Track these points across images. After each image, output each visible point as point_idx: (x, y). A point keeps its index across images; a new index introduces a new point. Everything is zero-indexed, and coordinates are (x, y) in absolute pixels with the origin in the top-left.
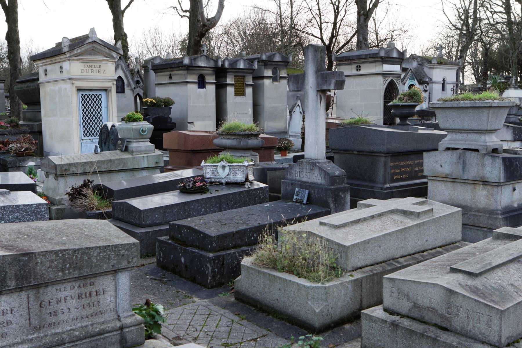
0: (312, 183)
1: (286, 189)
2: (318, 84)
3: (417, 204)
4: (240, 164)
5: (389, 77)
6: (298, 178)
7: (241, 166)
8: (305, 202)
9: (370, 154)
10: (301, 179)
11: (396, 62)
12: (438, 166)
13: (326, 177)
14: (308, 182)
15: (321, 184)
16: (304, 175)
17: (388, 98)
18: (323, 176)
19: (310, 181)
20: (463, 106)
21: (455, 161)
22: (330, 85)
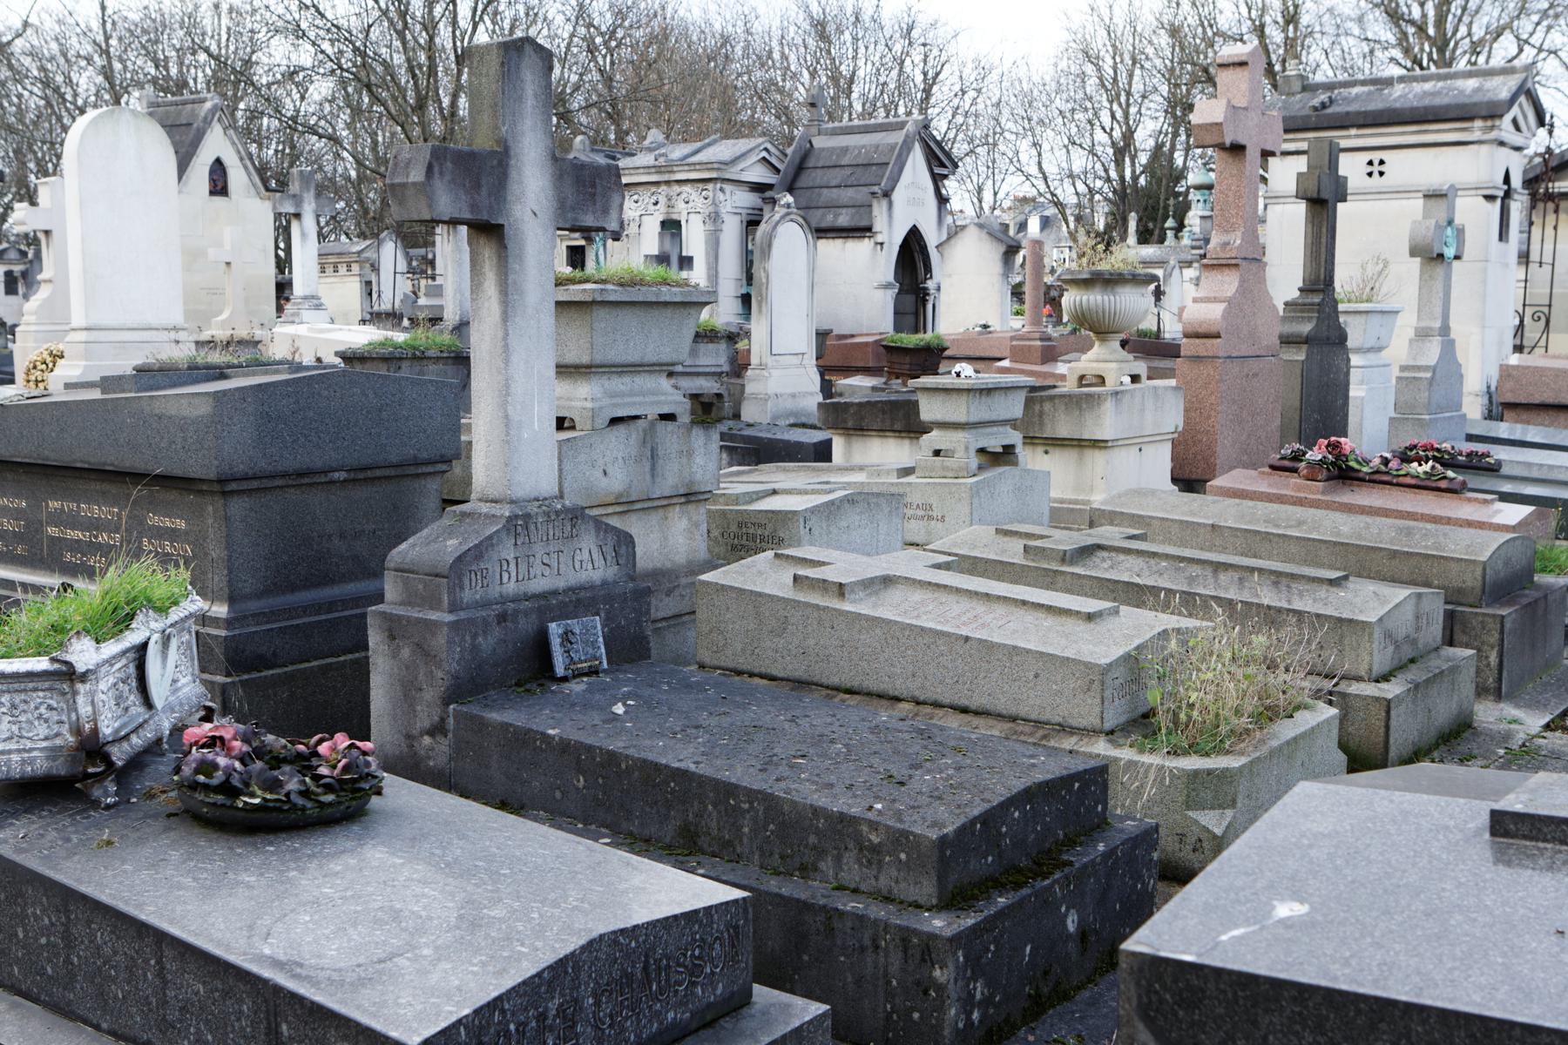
0: (571, 589)
1: (475, 648)
2: (562, 207)
3: (1042, 537)
6: (511, 587)
9: (399, 471)
12: (598, 474)
14: (555, 593)
15: (604, 583)
16: (538, 569)
18: (609, 550)
19: (561, 584)
20: (668, 299)
21: (633, 453)
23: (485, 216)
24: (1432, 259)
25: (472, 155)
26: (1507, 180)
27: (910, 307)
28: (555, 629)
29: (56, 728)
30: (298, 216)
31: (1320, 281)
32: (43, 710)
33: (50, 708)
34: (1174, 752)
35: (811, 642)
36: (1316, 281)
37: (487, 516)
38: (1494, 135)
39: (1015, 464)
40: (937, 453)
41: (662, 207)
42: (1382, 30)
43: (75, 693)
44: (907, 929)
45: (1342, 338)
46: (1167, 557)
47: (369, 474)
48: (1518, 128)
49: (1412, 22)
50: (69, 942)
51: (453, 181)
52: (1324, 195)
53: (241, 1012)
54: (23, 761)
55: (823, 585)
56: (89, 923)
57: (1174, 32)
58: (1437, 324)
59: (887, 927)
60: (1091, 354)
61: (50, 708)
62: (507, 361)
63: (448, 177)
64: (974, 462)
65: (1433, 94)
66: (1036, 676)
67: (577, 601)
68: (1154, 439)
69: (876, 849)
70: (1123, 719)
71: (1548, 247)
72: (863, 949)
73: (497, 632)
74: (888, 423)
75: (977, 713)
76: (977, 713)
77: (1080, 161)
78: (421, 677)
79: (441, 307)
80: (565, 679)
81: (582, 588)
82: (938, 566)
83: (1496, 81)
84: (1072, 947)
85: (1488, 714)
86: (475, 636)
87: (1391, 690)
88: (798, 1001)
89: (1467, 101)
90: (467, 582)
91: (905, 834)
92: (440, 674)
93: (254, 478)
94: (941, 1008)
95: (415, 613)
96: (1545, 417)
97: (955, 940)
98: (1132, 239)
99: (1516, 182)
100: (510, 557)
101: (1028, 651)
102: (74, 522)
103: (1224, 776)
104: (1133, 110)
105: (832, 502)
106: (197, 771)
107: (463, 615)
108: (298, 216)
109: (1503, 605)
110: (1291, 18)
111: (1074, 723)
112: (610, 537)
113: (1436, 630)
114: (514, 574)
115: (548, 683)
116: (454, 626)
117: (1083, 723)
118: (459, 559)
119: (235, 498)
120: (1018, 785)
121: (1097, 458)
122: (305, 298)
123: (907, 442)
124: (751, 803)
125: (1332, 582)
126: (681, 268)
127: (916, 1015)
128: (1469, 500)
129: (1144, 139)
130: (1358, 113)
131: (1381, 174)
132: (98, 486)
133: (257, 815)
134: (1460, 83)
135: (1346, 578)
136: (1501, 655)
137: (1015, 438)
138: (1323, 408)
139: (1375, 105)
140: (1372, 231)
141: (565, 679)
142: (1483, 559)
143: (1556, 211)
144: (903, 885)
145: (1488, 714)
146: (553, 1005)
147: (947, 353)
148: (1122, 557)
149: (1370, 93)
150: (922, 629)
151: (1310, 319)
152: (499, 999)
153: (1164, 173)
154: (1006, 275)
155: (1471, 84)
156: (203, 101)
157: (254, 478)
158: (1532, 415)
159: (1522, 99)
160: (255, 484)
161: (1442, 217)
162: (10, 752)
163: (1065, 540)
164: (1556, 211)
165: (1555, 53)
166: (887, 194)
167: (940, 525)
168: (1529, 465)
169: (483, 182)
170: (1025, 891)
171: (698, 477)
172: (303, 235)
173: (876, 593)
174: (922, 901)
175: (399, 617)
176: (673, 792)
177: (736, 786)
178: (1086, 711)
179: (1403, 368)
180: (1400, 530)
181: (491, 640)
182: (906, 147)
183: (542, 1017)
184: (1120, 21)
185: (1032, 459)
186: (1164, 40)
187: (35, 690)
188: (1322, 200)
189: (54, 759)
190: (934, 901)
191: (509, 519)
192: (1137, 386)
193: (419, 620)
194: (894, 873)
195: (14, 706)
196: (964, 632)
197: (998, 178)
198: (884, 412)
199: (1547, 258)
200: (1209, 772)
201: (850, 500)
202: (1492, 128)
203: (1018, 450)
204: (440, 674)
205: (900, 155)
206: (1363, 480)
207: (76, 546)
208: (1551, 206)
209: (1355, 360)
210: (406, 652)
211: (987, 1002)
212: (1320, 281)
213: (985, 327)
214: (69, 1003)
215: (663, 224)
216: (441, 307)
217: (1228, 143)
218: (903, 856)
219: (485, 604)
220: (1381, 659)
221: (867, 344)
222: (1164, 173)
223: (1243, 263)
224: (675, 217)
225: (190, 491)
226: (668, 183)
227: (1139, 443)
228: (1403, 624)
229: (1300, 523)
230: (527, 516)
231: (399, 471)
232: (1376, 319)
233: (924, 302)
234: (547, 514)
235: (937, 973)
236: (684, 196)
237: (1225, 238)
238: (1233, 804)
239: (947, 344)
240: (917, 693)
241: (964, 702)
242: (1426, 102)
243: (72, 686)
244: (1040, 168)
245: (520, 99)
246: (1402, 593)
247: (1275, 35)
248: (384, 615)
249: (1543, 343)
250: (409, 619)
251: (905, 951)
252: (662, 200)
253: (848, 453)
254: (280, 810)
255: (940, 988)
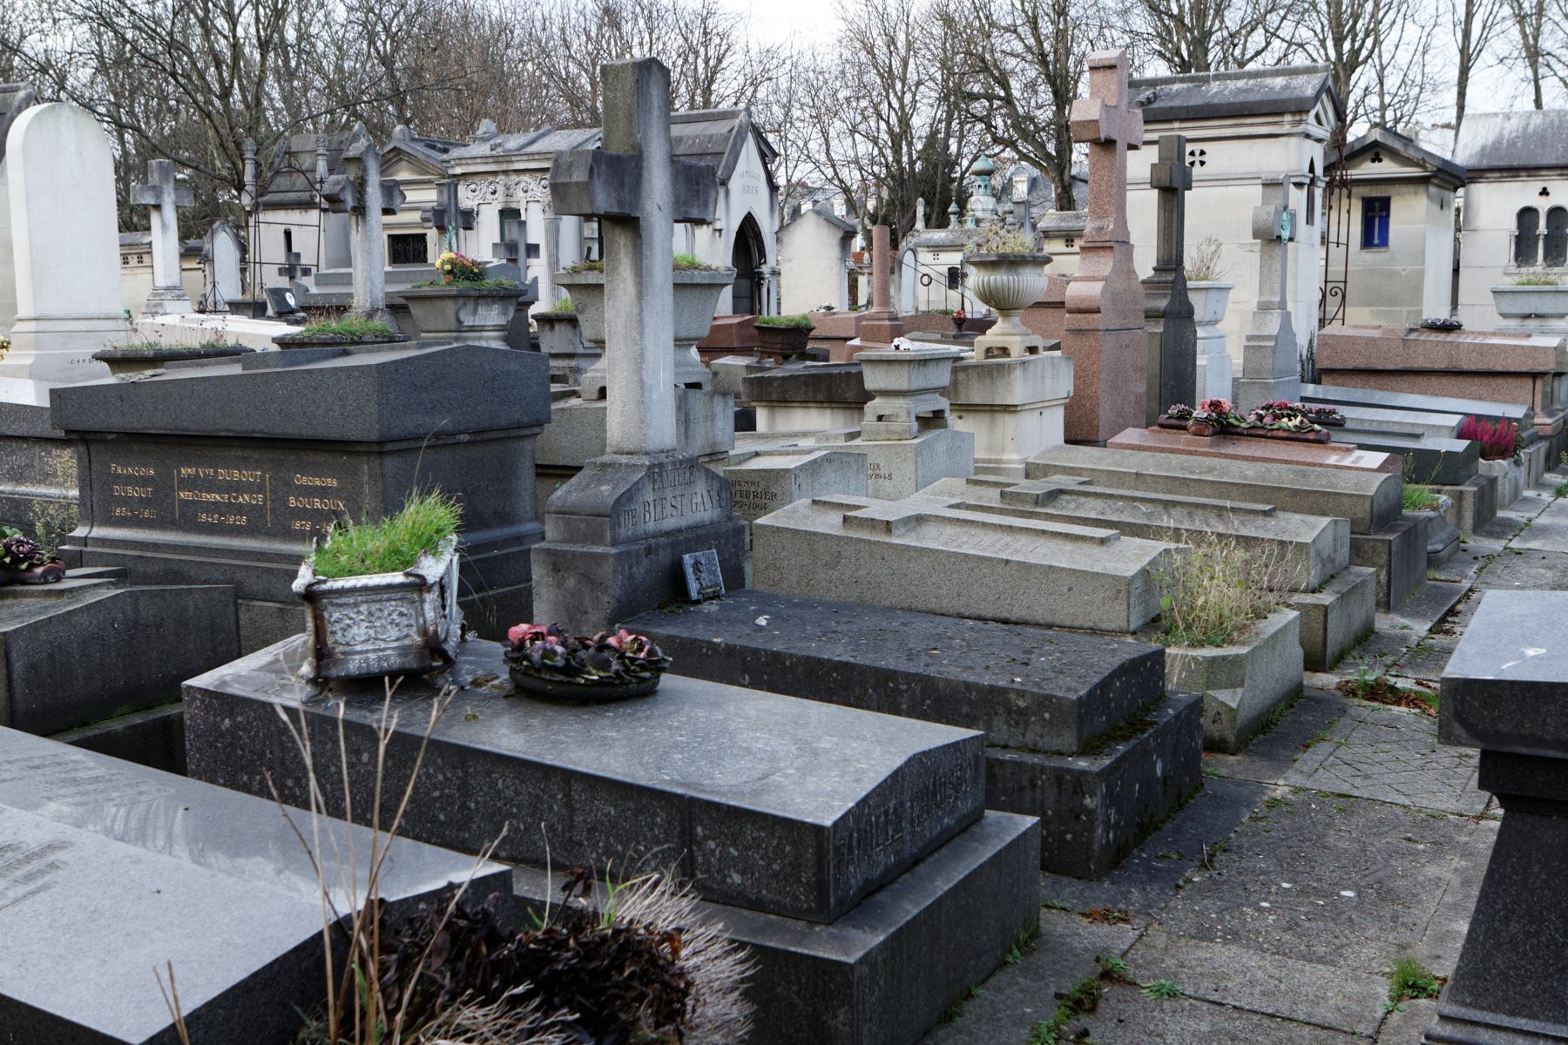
0: (690, 528)
1: (631, 577)
3: (859, 507)
6: (651, 526)
9: (505, 434)
14: (679, 530)
15: (712, 523)
16: (669, 510)
18: (714, 493)
19: (683, 523)
23: (627, 210)
24: (1271, 241)
25: (619, 158)
26: (1312, 169)
27: (745, 292)
29: (405, 631)
30: (158, 207)
31: (1171, 261)
32: (395, 616)
33: (401, 614)
34: (1192, 645)
35: (863, 572)
36: (1169, 261)
37: (627, 466)
38: (1301, 128)
39: (945, 426)
40: (880, 418)
41: (500, 195)
42: (1141, 21)
43: (423, 601)
44: (1061, 769)
45: (1190, 312)
46: (1122, 497)
47: (485, 436)
48: (1319, 122)
49: (1171, 16)
50: (465, 791)
52: (1175, 185)
53: (654, 824)
54: (379, 659)
55: (871, 523)
56: (489, 774)
57: (948, 21)
58: (1277, 299)
59: (1043, 769)
60: (994, 329)
61: (401, 614)
62: (642, 334)
64: (915, 426)
65: (1247, 91)
66: (1070, 589)
67: (696, 537)
68: (1050, 404)
69: (1023, 712)
70: (1141, 622)
71: (1344, 228)
72: (1021, 789)
73: (645, 562)
74: (811, 394)
75: (1016, 623)
76: (1016, 623)
77: (864, 148)
78: (587, 602)
79: (351, 295)
80: (698, 602)
82: (951, 506)
83: (1299, 81)
84: (1159, 788)
85: (1385, 623)
86: (631, 567)
87: (1326, 598)
88: (1018, 817)
89: (1277, 97)
91: (1049, 697)
92: (606, 599)
93: (406, 439)
94: (1091, 828)
95: (579, 548)
96: (1358, 380)
97: (1100, 774)
98: (920, 225)
99: (1319, 171)
101: (1062, 569)
102: (211, 485)
103: (1236, 661)
104: (908, 97)
105: (815, 461)
106: (543, 657)
107: (622, 548)
108: (158, 207)
109: (1387, 532)
110: (1062, 12)
111: (1103, 626)
113: (1345, 551)
115: (686, 607)
116: (618, 556)
117: (1111, 626)
118: (618, 501)
120: (1116, 662)
121: (1007, 421)
122: (168, 289)
123: (828, 412)
124: (909, 684)
125: (1265, 513)
126: (528, 256)
127: (1069, 837)
128: (1334, 449)
129: (921, 123)
130: (1181, 108)
131: (1202, 163)
132: (239, 453)
133: (597, 689)
134: (1269, 81)
135: (1274, 510)
136: (1389, 574)
137: (943, 403)
138: (1176, 375)
139: (1194, 101)
140: (1221, 211)
141: (698, 602)
142: (1371, 493)
143: (1349, 197)
144: (1047, 738)
145: (1385, 623)
146: (892, 804)
147: (813, 334)
148: (1082, 500)
149: (1189, 89)
150: (966, 555)
151: (1165, 295)
152: (867, 797)
153: (938, 158)
154: (843, 260)
155: (1279, 82)
156: (16, 90)
157: (406, 439)
158: (1347, 379)
159: (1324, 96)
161: (1279, 202)
162: (367, 651)
163: (1038, 487)
164: (1349, 197)
165: (1301, 46)
166: (724, 183)
167: (887, 482)
168: (1362, 421)
170: (1133, 741)
171: (719, 439)
172: (164, 226)
173: (914, 529)
174: (1063, 750)
175: (564, 553)
176: (835, 680)
177: (895, 672)
178: (1115, 615)
179: (1249, 338)
180: (1296, 473)
181: (642, 570)
182: (740, 138)
183: (886, 813)
184: (893, 12)
185: (956, 423)
186: (938, 30)
187: (389, 600)
188: (1172, 189)
189: (406, 655)
190: (1075, 749)
191: (650, 467)
192: (1033, 357)
193: (584, 554)
194: (1039, 729)
195: (371, 614)
196: (1004, 556)
197: (791, 165)
198: (806, 385)
199: (1343, 239)
200: (1224, 658)
201: (827, 459)
202: (1300, 122)
203: (947, 414)
204: (606, 599)
205: (734, 145)
206: (1241, 434)
207: (213, 507)
208: (1345, 191)
209: (1200, 333)
210: (571, 582)
211: (1116, 826)
212: (1171, 261)
213: (829, 308)
214: (465, 840)
215: (502, 212)
216: (351, 295)
217: (1103, 137)
218: (1047, 716)
219: (635, 539)
220: (1313, 577)
221: (731, 326)
222: (938, 158)
223: (1117, 246)
224: (514, 206)
225: (343, 453)
226: (506, 172)
227: (1039, 407)
228: (1326, 546)
229: (1211, 470)
230: (661, 465)
231: (505, 434)
232: (1213, 295)
233: (759, 286)
234: (674, 463)
235: (1088, 801)
236: (522, 185)
237: (1099, 224)
238: (1241, 684)
239: (814, 324)
240: (962, 610)
241: (1006, 615)
242: (1241, 98)
243: (421, 595)
244: (828, 153)
245: (649, 111)
246: (1324, 521)
247: (1046, 28)
248: (548, 552)
249: (1340, 315)
250: (574, 554)
251: (1059, 787)
252: (501, 189)
253: (772, 421)
254: (613, 684)
255: (1090, 813)
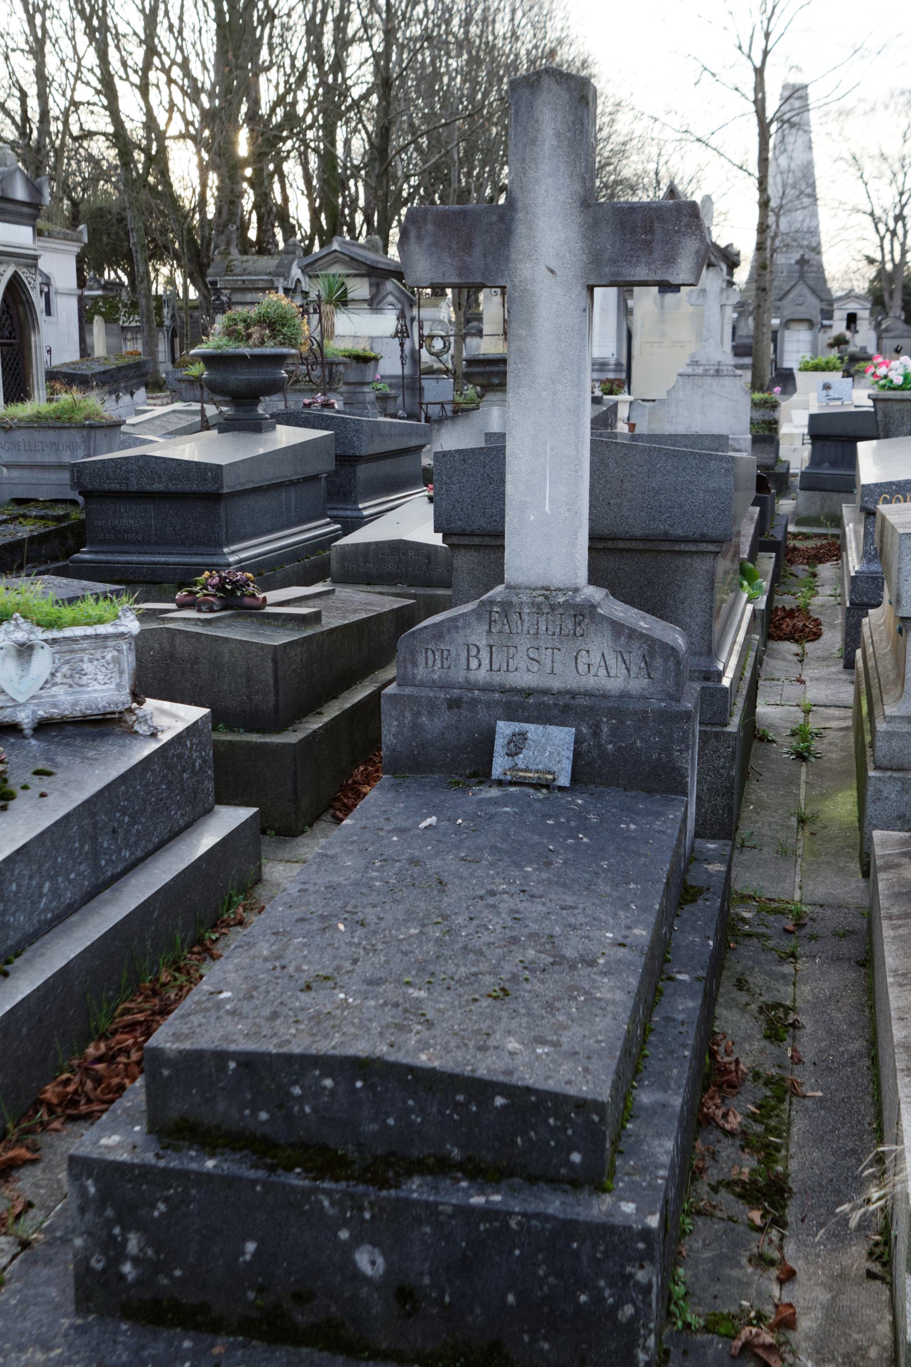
4: (102, 629)
5: (8, 264)
6: (482, 675)
7: (106, 637)
8: (564, 780)
9: (649, 546)
10: (497, 678)
11: (21, 215)
13: (659, 662)
14: (546, 692)
15: (624, 695)
16: (520, 661)
17: (7, 333)
19: (556, 684)
22: (670, 260)
28: (504, 729)
47: (610, 544)
51: (435, 244)
63: (428, 240)
81: (587, 694)
86: (417, 715)
90: (421, 659)
93: (472, 534)
100: (483, 643)
107: (408, 691)
112: (635, 645)
114: (486, 662)
119: (463, 552)
157: (472, 534)
160: (477, 541)
169: (477, 240)
